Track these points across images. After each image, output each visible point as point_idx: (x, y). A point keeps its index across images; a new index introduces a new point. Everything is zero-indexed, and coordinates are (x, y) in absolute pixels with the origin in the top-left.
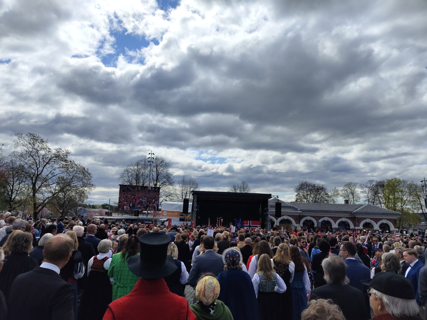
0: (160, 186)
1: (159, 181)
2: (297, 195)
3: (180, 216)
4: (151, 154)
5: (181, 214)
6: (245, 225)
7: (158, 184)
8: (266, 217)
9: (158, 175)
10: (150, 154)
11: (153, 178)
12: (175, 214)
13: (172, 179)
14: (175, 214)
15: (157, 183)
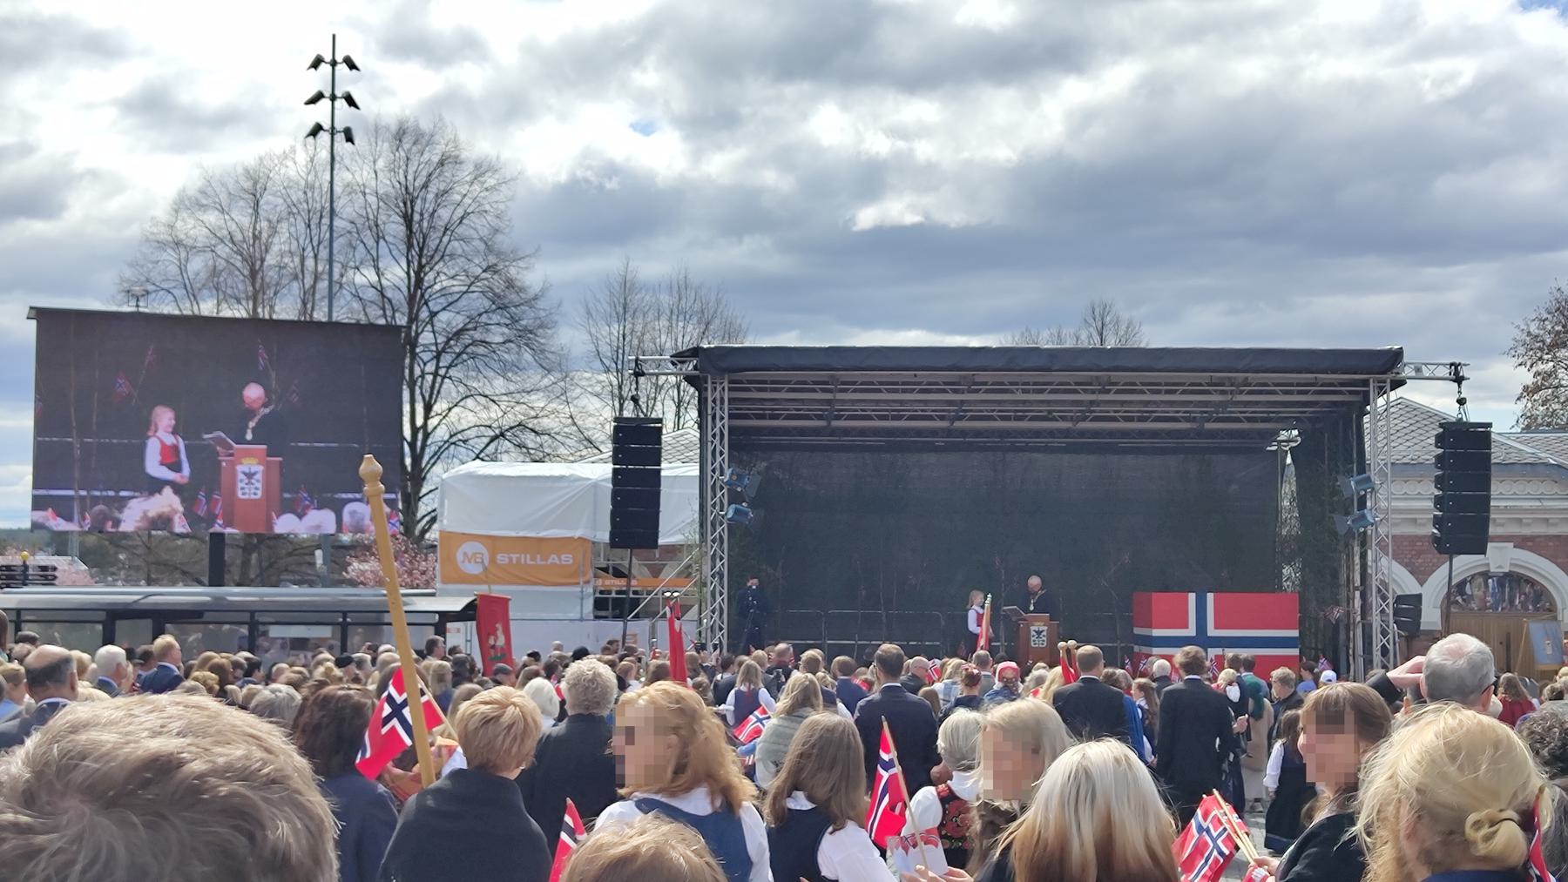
0: (444, 350)
1: (433, 314)
2: (1529, 391)
3: (596, 576)
4: (334, 63)
5: (603, 564)
6: (1156, 633)
7: (421, 340)
8: (1350, 556)
9: (421, 267)
10: (325, 68)
11: (383, 296)
12: (553, 559)
13: (531, 293)
14: (553, 559)
15: (418, 335)
